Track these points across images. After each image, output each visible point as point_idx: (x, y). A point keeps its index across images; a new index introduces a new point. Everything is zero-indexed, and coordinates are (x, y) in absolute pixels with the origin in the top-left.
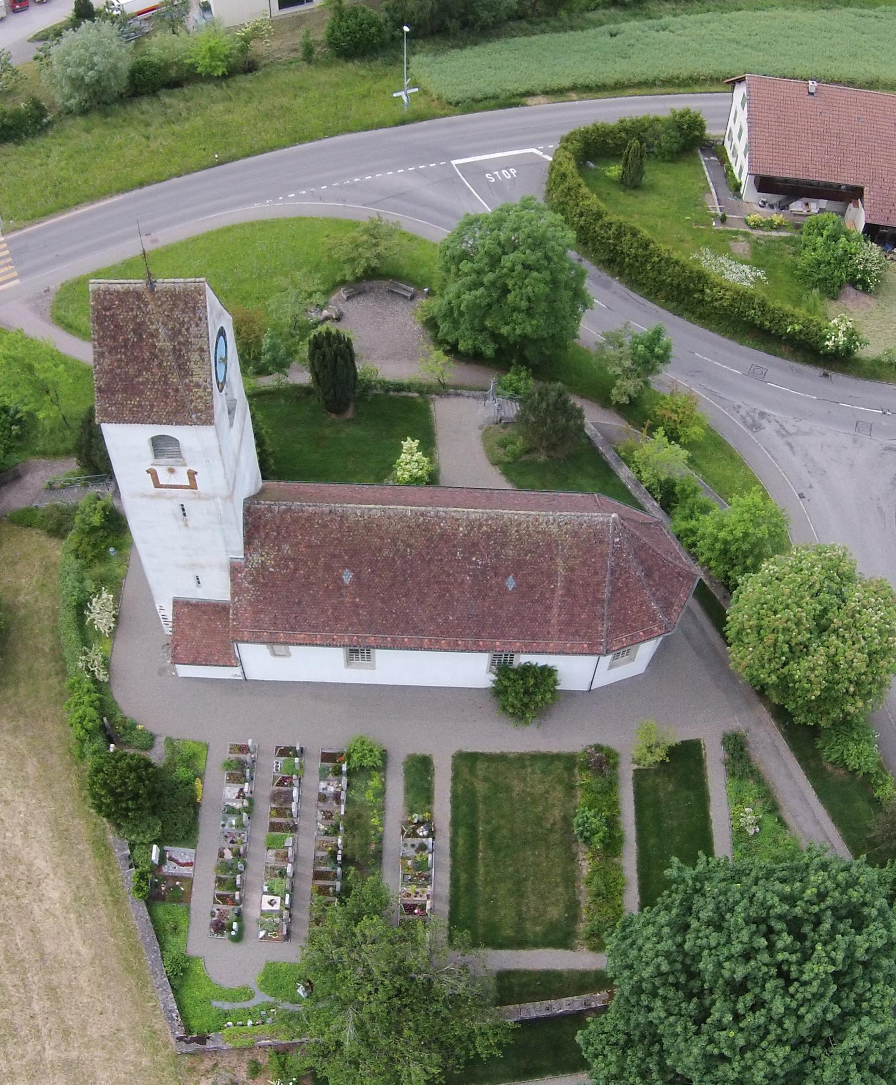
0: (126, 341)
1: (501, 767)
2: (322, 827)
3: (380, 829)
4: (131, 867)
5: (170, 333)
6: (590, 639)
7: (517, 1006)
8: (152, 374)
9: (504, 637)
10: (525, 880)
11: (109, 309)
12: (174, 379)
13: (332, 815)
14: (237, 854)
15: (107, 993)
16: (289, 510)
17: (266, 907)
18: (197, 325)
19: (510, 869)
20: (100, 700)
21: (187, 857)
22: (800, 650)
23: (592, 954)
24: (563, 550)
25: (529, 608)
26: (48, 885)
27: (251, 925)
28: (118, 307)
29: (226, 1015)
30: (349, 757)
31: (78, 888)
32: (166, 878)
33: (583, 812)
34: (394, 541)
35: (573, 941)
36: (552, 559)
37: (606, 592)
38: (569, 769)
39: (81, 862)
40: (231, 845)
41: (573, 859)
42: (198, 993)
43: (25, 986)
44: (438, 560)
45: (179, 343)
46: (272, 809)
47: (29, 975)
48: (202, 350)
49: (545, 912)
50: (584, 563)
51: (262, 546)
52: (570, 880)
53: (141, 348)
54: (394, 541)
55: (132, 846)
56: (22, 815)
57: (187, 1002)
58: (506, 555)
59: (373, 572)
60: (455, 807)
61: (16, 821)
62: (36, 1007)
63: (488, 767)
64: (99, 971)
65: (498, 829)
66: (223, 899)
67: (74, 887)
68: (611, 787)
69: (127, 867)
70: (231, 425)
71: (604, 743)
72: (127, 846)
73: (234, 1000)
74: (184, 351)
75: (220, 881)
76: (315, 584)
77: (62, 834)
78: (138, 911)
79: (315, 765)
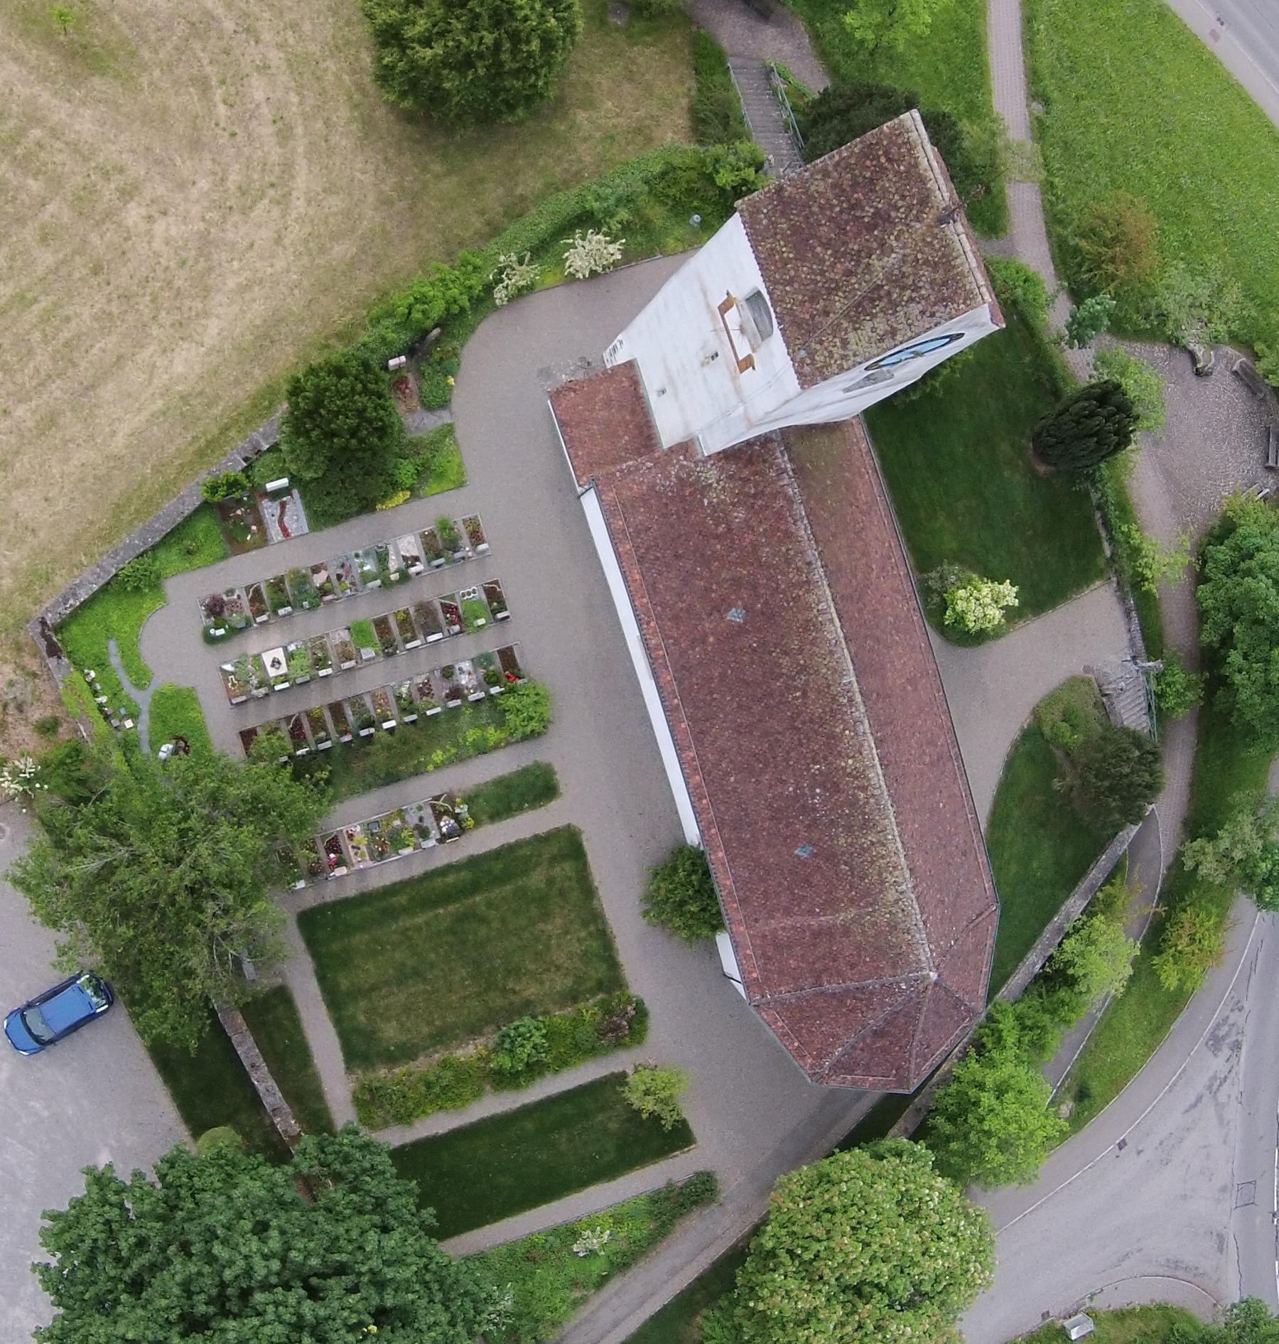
0: (857, 206)
1: (575, 895)
2: (404, 690)
3: (430, 767)
4: (246, 459)
5: (896, 272)
6: (767, 979)
7: (245, 1027)
8: (833, 265)
9: (732, 860)
10: (425, 980)
11: (889, 160)
12: (839, 303)
13: (427, 695)
14: (323, 591)
15: (76, 495)
16: (790, 501)
17: (267, 659)
18: (922, 313)
19: (432, 956)
20: (462, 310)
21: (294, 526)
22: (809, 1273)
23: (350, 1097)
24: (869, 914)
25: (780, 884)
26: (188, 350)
27: (234, 649)
28: (897, 173)
29: (101, 665)
30: (512, 691)
31: (201, 393)
32: (255, 510)
33: (538, 1029)
34: (803, 669)
35: (359, 1067)
36: (852, 901)
37: (830, 986)
38: (600, 986)
39: (237, 382)
40: (334, 578)
41: (472, 1032)
42: (115, 618)
43: (42, 384)
44: (799, 740)
45: (889, 294)
46: (406, 612)
47: (58, 382)
48: (893, 332)
49: (388, 1020)
50: (858, 947)
51: (730, 477)
52: (442, 1037)
53: (858, 234)
54: (803, 669)
55: (274, 448)
56: (269, 270)
57: (98, 609)
58: (837, 836)
59: (754, 650)
60: (497, 854)
61: (258, 265)
62: (20, 411)
63: (570, 879)
64: (102, 471)
65: (483, 920)
66: (256, 597)
67: (199, 389)
68: (592, 1051)
69: (244, 455)
70: (847, 390)
71: (653, 1021)
72: (272, 441)
73: (127, 668)
74: (882, 304)
75: (277, 585)
76: (711, 571)
77: (265, 337)
78: (191, 495)
79: (491, 643)
